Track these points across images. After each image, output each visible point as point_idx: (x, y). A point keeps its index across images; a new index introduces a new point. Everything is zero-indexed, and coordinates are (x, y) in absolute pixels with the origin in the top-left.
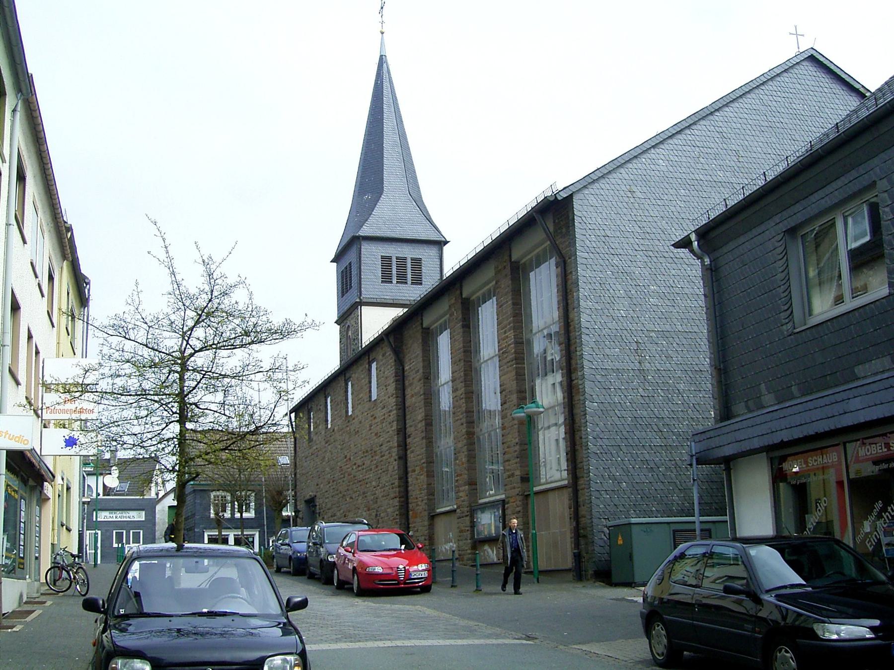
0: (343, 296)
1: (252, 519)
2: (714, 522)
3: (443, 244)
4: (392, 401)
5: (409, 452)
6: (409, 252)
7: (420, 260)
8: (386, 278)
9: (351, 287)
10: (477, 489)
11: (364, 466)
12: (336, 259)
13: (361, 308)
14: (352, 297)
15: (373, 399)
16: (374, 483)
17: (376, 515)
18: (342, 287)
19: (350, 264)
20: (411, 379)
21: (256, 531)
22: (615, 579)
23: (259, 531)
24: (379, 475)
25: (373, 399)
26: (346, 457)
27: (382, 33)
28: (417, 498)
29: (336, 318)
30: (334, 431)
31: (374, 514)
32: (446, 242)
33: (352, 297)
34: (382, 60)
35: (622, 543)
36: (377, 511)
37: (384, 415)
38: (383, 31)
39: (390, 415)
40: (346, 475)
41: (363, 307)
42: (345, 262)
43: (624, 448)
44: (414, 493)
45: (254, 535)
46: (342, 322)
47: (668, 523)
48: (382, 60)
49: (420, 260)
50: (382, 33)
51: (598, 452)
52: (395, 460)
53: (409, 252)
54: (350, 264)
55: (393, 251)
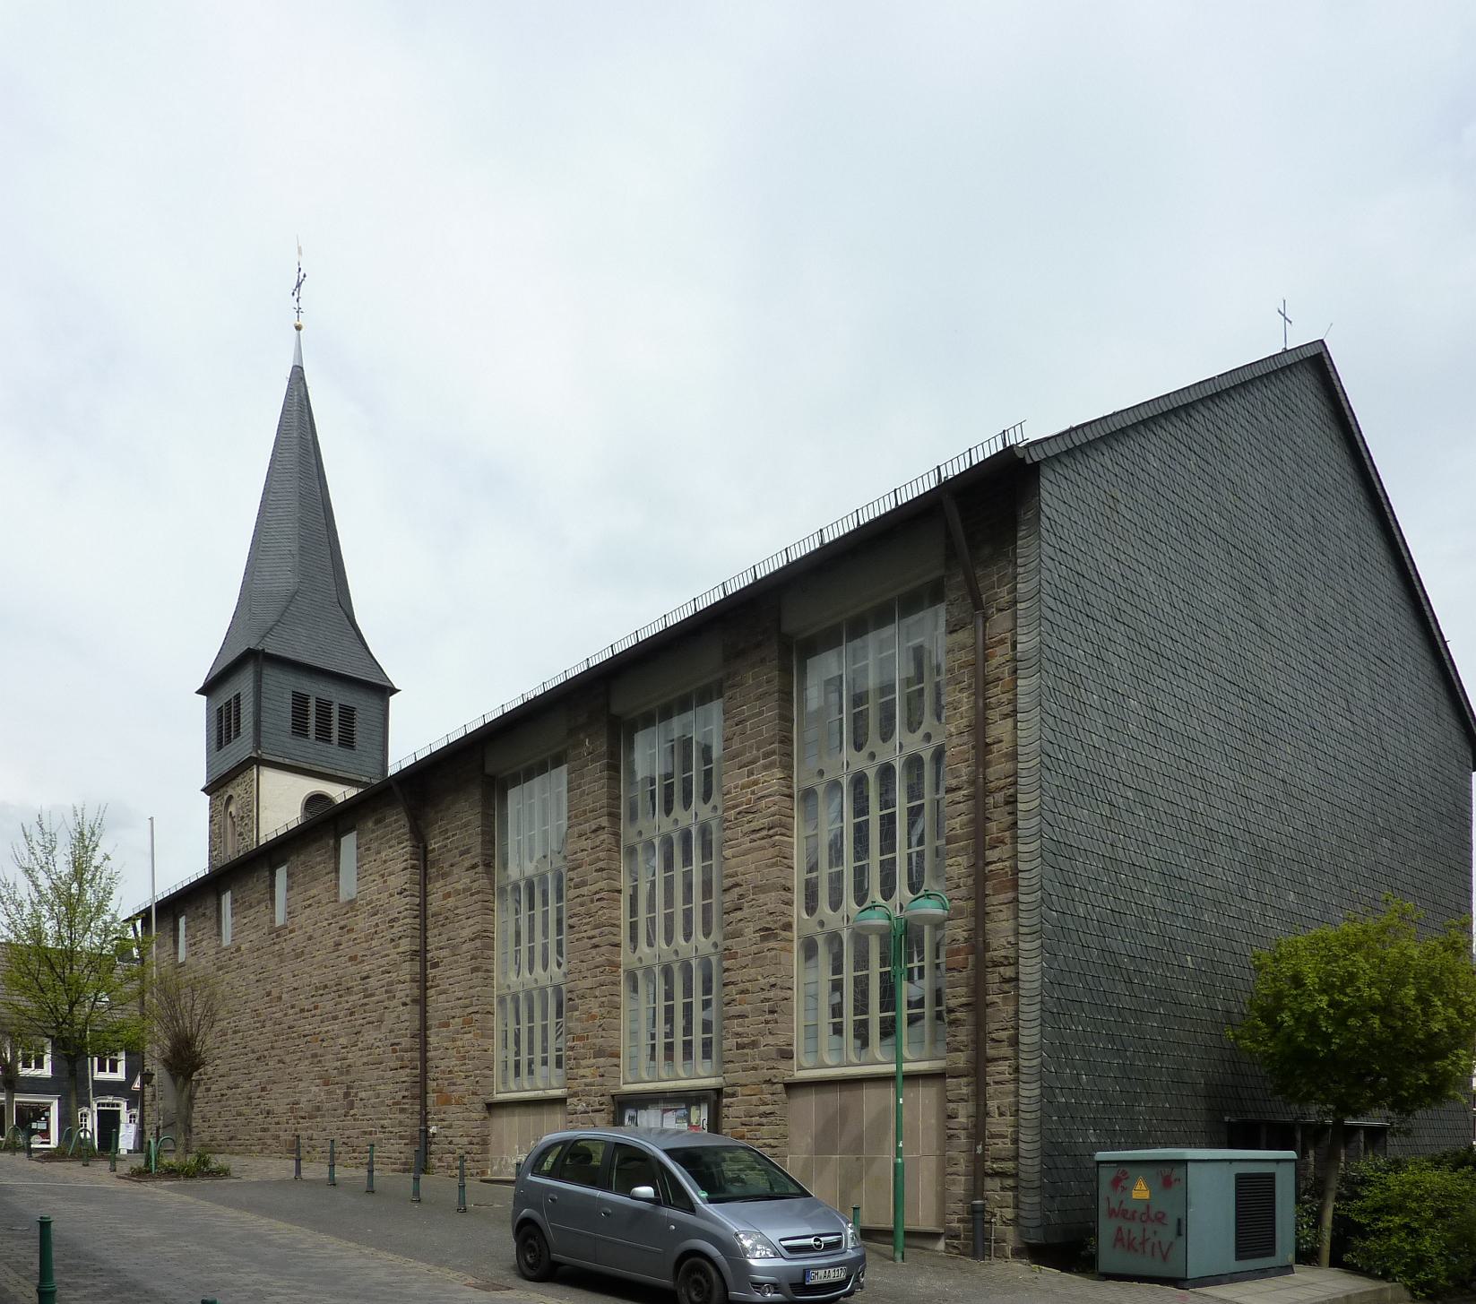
0: (220, 747)
1: (47, 1079)
2: (1278, 1161)
3: (385, 692)
4: (401, 903)
5: (431, 992)
6: (338, 697)
7: (353, 709)
8: (299, 728)
9: (238, 734)
10: (618, 1066)
11: (318, 1012)
12: (208, 689)
13: (258, 771)
14: (242, 748)
15: (343, 897)
16: (343, 1041)
17: (347, 1095)
18: (220, 732)
19: (238, 697)
20: (446, 865)
21: (55, 1098)
22: (1109, 1257)
23: (59, 1099)
24: (358, 1029)
25: (343, 897)
26: (269, 994)
27: (298, 328)
28: (450, 1072)
29: (204, 784)
30: (238, 949)
31: (340, 1092)
32: (394, 691)
33: (242, 748)
34: (298, 376)
35: (1147, 1197)
36: (348, 1087)
37: (377, 925)
38: (301, 322)
39: (392, 927)
40: (268, 1023)
41: (261, 767)
42: (226, 694)
43: (1086, 1007)
44: (443, 1064)
45: (50, 1104)
46: (217, 790)
47: (1231, 1161)
48: (298, 376)
49: (353, 709)
50: (298, 328)
51: (1055, 1010)
52: (405, 1004)
53: (338, 697)
54: (238, 697)
55: (315, 690)
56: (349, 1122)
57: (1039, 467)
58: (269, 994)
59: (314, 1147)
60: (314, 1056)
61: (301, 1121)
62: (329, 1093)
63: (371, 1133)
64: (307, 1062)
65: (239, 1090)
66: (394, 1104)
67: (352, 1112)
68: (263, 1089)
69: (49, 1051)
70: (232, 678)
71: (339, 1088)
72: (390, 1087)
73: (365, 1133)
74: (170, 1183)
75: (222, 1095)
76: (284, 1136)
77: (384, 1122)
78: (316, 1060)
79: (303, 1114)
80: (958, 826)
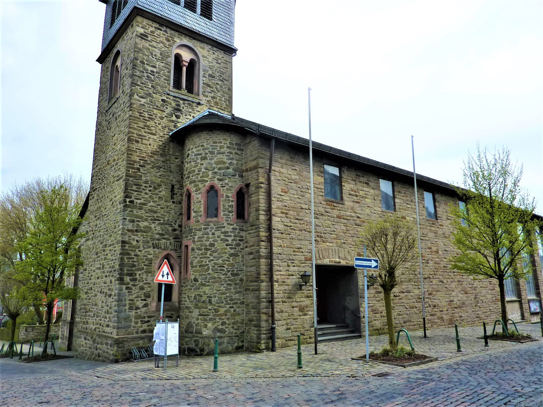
17: (475, 298)
56: (477, 308)
57: (241, 218)
58: (430, 248)
59: (463, 320)
60: (459, 281)
61: (456, 309)
62: (467, 297)
63: (486, 312)
64: (455, 284)
65: (411, 294)
66: (493, 302)
67: (479, 305)
68: (430, 294)
69: (539, 241)
70: (219, 132)
71: (471, 295)
72: (490, 296)
73: (484, 312)
74: (416, 368)
75: (283, 282)
76: (445, 317)
77: (491, 308)
78: (460, 283)
79: (456, 306)
80: (234, 244)
